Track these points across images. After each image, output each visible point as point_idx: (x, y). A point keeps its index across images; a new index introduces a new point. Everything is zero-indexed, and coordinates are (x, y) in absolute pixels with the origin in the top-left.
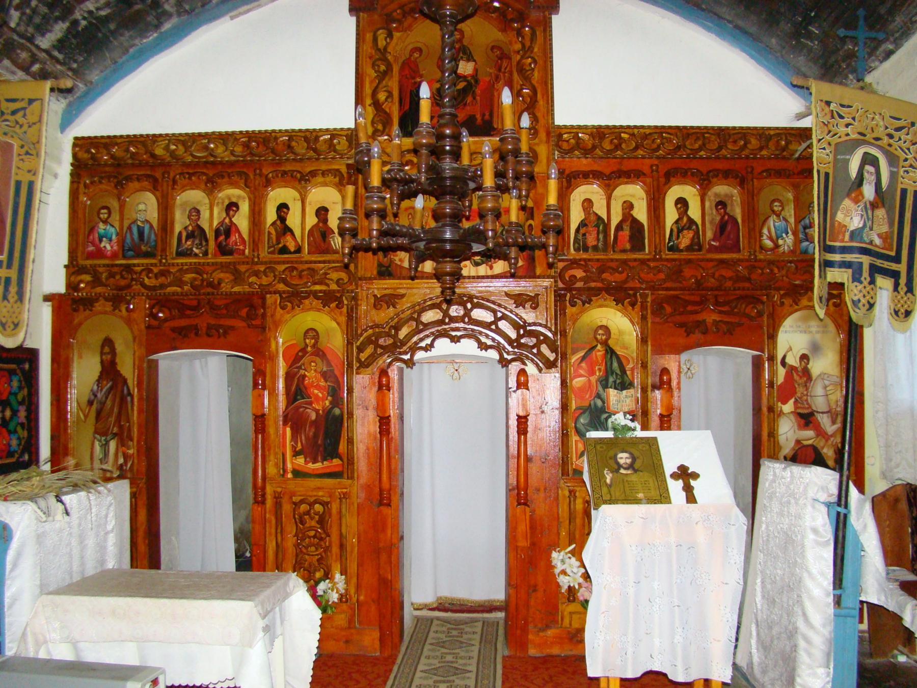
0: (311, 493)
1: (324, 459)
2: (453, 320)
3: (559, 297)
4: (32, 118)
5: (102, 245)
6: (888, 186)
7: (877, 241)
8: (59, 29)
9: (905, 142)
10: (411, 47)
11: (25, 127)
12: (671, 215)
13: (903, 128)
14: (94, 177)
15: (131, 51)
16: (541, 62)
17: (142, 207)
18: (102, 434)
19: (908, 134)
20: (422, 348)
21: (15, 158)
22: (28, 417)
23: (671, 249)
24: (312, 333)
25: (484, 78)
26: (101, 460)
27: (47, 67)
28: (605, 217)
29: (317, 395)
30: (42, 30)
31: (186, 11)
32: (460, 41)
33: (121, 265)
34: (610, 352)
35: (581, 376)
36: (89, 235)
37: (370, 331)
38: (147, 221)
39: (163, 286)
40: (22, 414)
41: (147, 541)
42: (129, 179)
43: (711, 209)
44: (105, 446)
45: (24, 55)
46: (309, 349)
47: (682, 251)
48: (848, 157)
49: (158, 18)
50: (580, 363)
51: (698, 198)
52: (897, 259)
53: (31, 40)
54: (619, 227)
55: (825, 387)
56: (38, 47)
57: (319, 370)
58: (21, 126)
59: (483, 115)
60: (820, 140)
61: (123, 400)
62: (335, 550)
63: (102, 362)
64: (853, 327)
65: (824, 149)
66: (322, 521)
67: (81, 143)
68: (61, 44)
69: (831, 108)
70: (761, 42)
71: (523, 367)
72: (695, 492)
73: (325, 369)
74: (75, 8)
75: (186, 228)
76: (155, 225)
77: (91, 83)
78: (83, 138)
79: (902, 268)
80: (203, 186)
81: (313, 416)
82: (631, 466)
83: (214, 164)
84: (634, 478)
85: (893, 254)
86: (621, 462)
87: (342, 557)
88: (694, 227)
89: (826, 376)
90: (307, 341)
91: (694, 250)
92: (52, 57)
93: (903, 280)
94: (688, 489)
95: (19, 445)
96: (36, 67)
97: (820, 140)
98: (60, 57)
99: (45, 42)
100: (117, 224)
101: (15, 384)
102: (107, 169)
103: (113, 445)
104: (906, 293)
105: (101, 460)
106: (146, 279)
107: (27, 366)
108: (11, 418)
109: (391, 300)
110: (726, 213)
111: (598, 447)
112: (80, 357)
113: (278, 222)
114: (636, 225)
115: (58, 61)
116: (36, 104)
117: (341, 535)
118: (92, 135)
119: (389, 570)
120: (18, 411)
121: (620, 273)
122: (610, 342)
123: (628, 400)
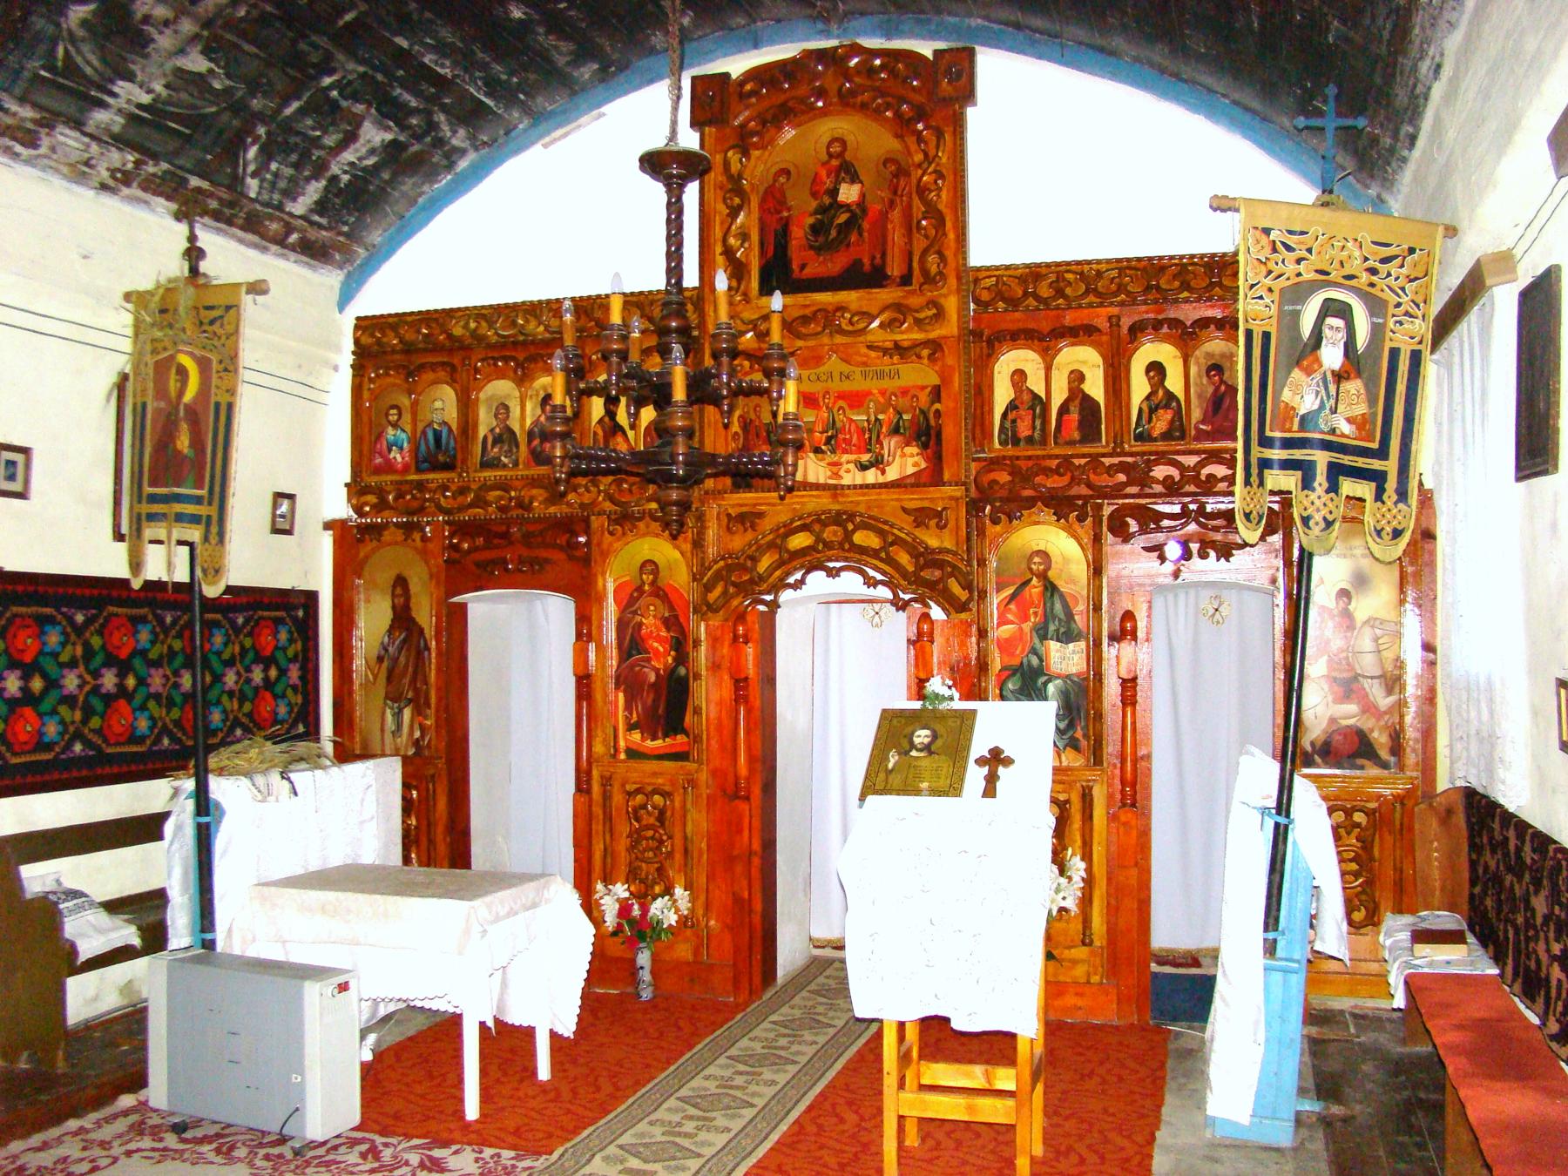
0: (647, 780)
1: (666, 735)
2: (828, 545)
3: (975, 507)
4: (230, 328)
5: (392, 456)
6: (1368, 346)
7: (1346, 428)
8: (313, 191)
9: (1396, 279)
10: (773, 170)
11: (224, 338)
12: (1139, 388)
13: (1396, 257)
14: (378, 369)
15: (421, 200)
16: (950, 178)
17: (438, 404)
18: (394, 700)
19: (1402, 266)
20: (790, 586)
21: (215, 376)
22: (302, 678)
23: (1139, 437)
24: (650, 566)
25: (875, 206)
26: (393, 732)
27: (308, 235)
28: (1043, 396)
29: (657, 649)
30: (292, 194)
31: (485, 143)
32: (841, 155)
33: (412, 481)
34: (1050, 588)
35: (1011, 622)
36: (376, 443)
37: (722, 563)
38: (445, 423)
39: (462, 509)
40: (294, 673)
41: (448, 839)
42: (423, 366)
43: (1200, 377)
44: (398, 715)
45: (274, 227)
46: (647, 587)
47: (1155, 440)
48: (1299, 307)
49: (447, 156)
50: (1009, 603)
51: (1180, 362)
52: (1382, 453)
53: (280, 207)
54: (1064, 409)
55: (1376, 639)
56: (291, 214)
57: (659, 616)
58: (220, 338)
59: (873, 258)
60: (1252, 286)
61: (419, 654)
62: (678, 856)
63: (394, 607)
64: (1306, 555)
65: (1261, 298)
66: (661, 817)
67: (365, 325)
68: (321, 206)
69: (1272, 238)
70: (1272, 122)
71: (926, 610)
72: (998, 784)
73: (667, 615)
74: (329, 162)
75: (492, 430)
76: (454, 426)
77: (374, 246)
78: (366, 318)
79: (1391, 466)
80: (512, 374)
81: (652, 677)
82: (927, 748)
83: (524, 344)
84: (924, 763)
85: (1375, 445)
86: (917, 741)
87: (685, 868)
88: (1174, 404)
89: (1378, 622)
90: (644, 577)
91: (1173, 439)
92: (312, 223)
93: (1391, 484)
94: (991, 779)
95: (290, 713)
96: (294, 238)
97: (1252, 286)
98: (324, 221)
99: (299, 207)
100: (408, 428)
101: (283, 636)
102: (397, 357)
103: (407, 713)
104: (1396, 503)
105: (393, 732)
106: (442, 499)
107: (301, 613)
108: (278, 679)
109: (748, 519)
110: (1222, 381)
111: (895, 722)
112: (368, 601)
113: (607, 419)
114: (1088, 403)
115: (320, 226)
116: (232, 312)
117: (685, 838)
118: (378, 313)
119: (746, 887)
120: (224, 675)
121: (1061, 475)
122: (1050, 574)
123: (1076, 657)
